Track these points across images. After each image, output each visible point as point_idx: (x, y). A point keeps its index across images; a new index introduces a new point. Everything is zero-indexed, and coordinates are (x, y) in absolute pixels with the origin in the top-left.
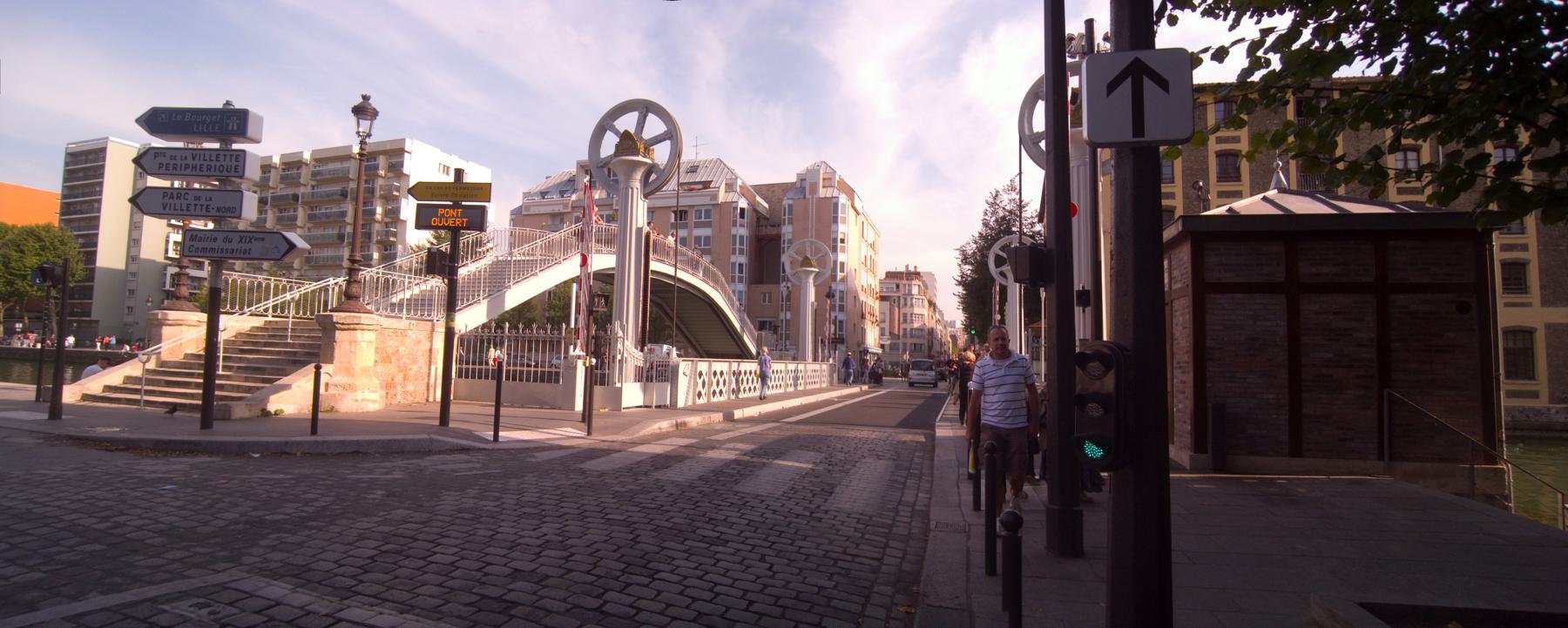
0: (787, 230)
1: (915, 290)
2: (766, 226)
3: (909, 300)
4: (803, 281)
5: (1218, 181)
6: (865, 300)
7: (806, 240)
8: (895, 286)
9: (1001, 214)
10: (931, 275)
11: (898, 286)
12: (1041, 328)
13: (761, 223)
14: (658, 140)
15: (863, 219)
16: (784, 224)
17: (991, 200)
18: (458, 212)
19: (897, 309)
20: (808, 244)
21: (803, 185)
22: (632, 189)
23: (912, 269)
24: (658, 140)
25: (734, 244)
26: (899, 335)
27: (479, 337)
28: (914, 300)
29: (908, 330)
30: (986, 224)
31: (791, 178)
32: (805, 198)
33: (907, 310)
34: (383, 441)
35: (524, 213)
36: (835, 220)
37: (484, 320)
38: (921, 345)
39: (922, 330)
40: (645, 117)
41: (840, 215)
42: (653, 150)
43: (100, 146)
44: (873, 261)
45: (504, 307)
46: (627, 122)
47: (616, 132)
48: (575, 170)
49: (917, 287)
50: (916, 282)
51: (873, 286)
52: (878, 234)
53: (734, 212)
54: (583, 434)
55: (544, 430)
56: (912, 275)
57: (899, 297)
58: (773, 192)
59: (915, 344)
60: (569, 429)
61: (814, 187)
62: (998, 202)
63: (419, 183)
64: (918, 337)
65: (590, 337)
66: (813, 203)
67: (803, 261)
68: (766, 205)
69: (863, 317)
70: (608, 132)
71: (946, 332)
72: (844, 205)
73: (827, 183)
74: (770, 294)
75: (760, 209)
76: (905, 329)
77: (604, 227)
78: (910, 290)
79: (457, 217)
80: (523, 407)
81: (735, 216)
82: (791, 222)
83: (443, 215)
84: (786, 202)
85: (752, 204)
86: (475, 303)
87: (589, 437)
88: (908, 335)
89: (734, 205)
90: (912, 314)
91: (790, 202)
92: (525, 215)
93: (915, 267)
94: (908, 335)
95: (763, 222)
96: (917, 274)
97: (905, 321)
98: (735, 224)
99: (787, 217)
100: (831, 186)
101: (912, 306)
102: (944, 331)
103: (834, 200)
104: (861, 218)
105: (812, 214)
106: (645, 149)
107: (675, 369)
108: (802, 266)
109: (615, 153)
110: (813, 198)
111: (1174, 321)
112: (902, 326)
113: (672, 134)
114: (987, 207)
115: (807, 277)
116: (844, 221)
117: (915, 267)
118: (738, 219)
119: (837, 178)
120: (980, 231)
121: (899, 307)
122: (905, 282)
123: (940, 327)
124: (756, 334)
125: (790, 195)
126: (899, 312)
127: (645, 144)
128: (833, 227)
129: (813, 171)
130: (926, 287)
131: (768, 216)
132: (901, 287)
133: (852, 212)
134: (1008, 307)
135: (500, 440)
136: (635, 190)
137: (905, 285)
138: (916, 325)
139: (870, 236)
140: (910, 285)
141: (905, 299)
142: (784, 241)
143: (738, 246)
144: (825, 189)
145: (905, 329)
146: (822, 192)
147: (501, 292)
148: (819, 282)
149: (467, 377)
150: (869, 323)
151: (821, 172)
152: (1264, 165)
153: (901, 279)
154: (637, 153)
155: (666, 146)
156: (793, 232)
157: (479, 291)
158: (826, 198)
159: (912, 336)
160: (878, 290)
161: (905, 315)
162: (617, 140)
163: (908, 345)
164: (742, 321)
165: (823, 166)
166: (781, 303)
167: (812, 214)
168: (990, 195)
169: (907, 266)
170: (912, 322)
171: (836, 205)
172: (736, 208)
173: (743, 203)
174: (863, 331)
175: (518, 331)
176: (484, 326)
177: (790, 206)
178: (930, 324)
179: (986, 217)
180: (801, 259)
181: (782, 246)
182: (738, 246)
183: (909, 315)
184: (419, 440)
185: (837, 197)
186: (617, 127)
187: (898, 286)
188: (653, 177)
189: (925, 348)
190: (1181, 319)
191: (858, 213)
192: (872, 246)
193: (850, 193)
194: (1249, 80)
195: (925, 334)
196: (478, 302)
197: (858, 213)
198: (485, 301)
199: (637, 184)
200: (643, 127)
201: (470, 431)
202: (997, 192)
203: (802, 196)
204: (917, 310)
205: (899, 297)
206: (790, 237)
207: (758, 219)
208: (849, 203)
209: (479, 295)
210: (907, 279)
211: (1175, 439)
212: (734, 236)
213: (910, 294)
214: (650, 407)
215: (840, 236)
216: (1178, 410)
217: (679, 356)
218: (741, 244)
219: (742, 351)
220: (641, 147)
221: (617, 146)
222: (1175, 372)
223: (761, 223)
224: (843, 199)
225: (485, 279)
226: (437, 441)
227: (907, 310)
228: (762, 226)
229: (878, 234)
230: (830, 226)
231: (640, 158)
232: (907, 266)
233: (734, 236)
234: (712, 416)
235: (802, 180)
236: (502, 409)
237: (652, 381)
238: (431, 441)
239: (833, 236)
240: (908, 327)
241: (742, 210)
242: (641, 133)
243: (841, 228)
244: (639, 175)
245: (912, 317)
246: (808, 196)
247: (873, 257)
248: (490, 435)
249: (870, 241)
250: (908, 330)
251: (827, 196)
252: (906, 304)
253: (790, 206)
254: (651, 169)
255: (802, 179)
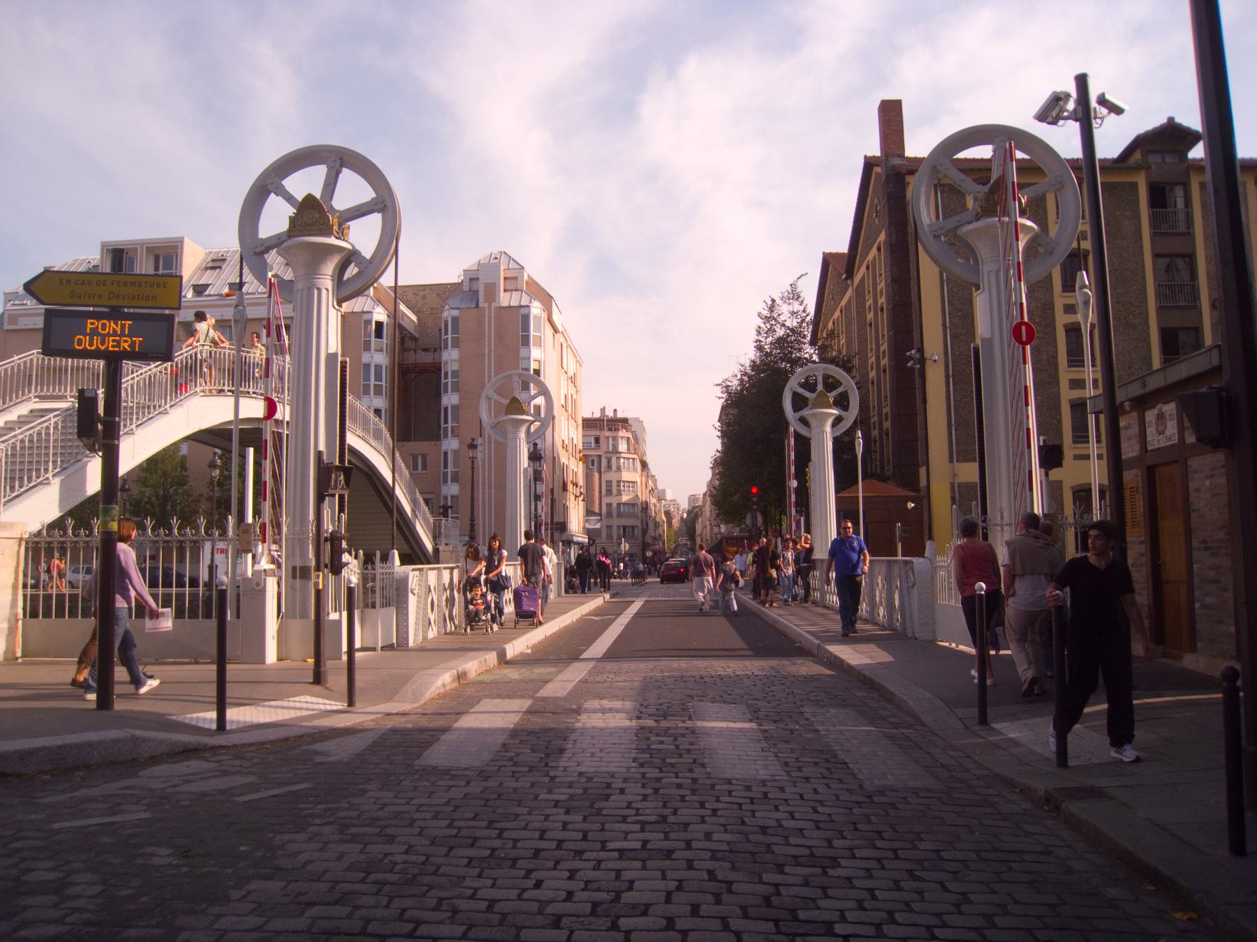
0: (451, 358)
1: (623, 447)
2: (415, 350)
3: (614, 460)
4: (510, 436)
5: (1063, 291)
6: (566, 463)
7: (513, 371)
8: (593, 440)
9: (780, 332)
10: (637, 420)
11: (597, 440)
12: (858, 497)
13: (406, 347)
14: (360, 212)
15: (562, 340)
16: (446, 347)
17: (766, 313)
18: (123, 326)
19: (597, 475)
20: (516, 379)
21: (474, 288)
22: (319, 290)
23: (610, 414)
24: (360, 212)
25: (367, 378)
26: (600, 514)
27: (43, 545)
28: (622, 460)
29: (614, 505)
30: (760, 348)
31: (452, 276)
32: (477, 306)
33: (611, 476)
34: (49, 749)
35: (6, 327)
36: (526, 341)
37: (54, 513)
38: (633, 527)
39: (633, 505)
40: (338, 173)
41: (532, 333)
42: (349, 228)
43: (913, 168)
44: (574, 402)
45: (86, 491)
46: (307, 182)
47: (289, 198)
48: (98, 257)
49: (625, 442)
50: (622, 433)
51: (575, 442)
52: (579, 363)
53: (366, 328)
54: (340, 705)
55: (273, 703)
56: (617, 423)
57: (600, 456)
58: (424, 297)
59: (624, 527)
60: (308, 698)
61: (491, 290)
62: (775, 315)
63: (47, 272)
64: (629, 516)
65: (322, 540)
66: (490, 317)
67: (509, 406)
68: (414, 318)
69: (565, 488)
70: (273, 195)
71: (660, 506)
72: (537, 318)
73: (510, 285)
74: (424, 456)
75: (405, 324)
76: (609, 505)
77: (227, 351)
78: (615, 446)
79: (123, 335)
80: (197, 663)
81: (367, 335)
82: (456, 344)
83: (94, 332)
84: (448, 314)
85: (394, 314)
86: (40, 483)
87: (350, 709)
88: (615, 513)
89: (366, 317)
90: (619, 482)
91: (455, 313)
92: (7, 330)
93: (615, 411)
94: (615, 513)
95: (409, 344)
96: (625, 422)
97: (609, 492)
98: (367, 347)
99: (449, 336)
100: (516, 290)
101: (619, 469)
102: (658, 505)
103: (523, 311)
104: (560, 338)
105: (490, 332)
106: (340, 225)
107: (404, 582)
108: (508, 413)
109: (289, 230)
110: (490, 307)
111: (1192, 486)
112: (605, 500)
113: (384, 204)
114: (760, 322)
115: (516, 431)
116: (539, 343)
117: (615, 411)
118: (373, 339)
119: (526, 277)
120: (753, 358)
121: (600, 473)
122: (607, 433)
123: (653, 500)
124: (432, 520)
125: (454, 302)
126: (600, 478)
127: (339, 218)
128: (523, 352)
129: (490, 265)
130: (636, 439)
131: (417, 335)
132: (602, 441)
133: (549, 330)
134: (812, 470)
135: (228, 727)
136: (324, 292)
137: (607, 438)
138: (625, 498)
139: (571, 367)
140: (615, 439)
141: (609, 461)
142: (446, 374)
143: (372, 382)
144: (508, 294)
145: (609, 505)
146: (505, 299)
147: (79, 465)
148: (838, 434)
149: (47, 614)
150: (572, 498)
151: (502, 268)
152: (1116, 270)
153: (602, 429)
154: (328, 233)
155: (374, 222)
156: (461, 361)
157: (47, 462)
158: (510, 307)
159: (619, 515)
160: (580, 446)
161: (609, 483)
162: (291, 211)
163: (615, 529)
164: (414, 502)
165: (504, 259)
166: (442, 470)
167: (490, 332)
168: (764, 305)
169: (603, 410)
170: (619, 493)
171: (526, 318)
172: (368, 322)
173: (380, 315)
174: (565, 508)
175: (65, 533)
176: (52, 526)
177: (455, 319)
178: (643, 496)
179: (760, 338)
180: (506, 402)
181: (443, 381)
182: (372, 382)
183: (614, 485)
184: (115, 742)
185: (528, 306)
186: (287, 188)
187: (597, 440)
188: (352, 271)
189: (638, 532)
190: (1208, 483)
191: (556, 330)
192: (573, 380)
193: (547, 300)
194: (955, 157)
195: (638, 510)
196: (46, 482)
197: (556, 330)
198: (56, 483)
199: (327, 283)
200: (333, 190)
201: (162, 715)
202: (773, 301)
203: (473, 305)
204: (626, 476)
205: (600, 456)
206: (455, 367)
207: (402, 339)
208: (544, 315)
209: (46, 470)
210: (610, 430)
211: (1199, 645)
212: (367, 366)
213: (616, 451)
214: (374, 649)
215: (534, 366)
216: (1205, 606)
217: (403, 562)
218: (378, 378)
219: (412, 548)
220: (334, 221)
221: (293, 220)
222: (1195, 554)
223: (406, 347)
224: (536, 309)
225: (55, 441)
226: (146, 740)
227: (611, 476)
228: (409, 350)
229: (579, 363)
230: (518, 351)
231: (332, 241)
232: (603, 410)
233: (367, 366)
234: (487, 657)
235: (471, 280)
236: (229, 667)
237: (374, 606)
238: (135, 740)
239: (523, 364)
240: (614, 501)
241: (379, 325)
242: (331, 199)
243: (535, 353)
244: (329, 268)
245: (619, 486)
246: (482, 304)
247: (574, 396)
248: (211, 721)
249: (571, 373)
250: (614, 505)
251: (512, 304)
252: (609, 467)
253: (455, 320)
254: (351, 256)
255: (472, 278)
